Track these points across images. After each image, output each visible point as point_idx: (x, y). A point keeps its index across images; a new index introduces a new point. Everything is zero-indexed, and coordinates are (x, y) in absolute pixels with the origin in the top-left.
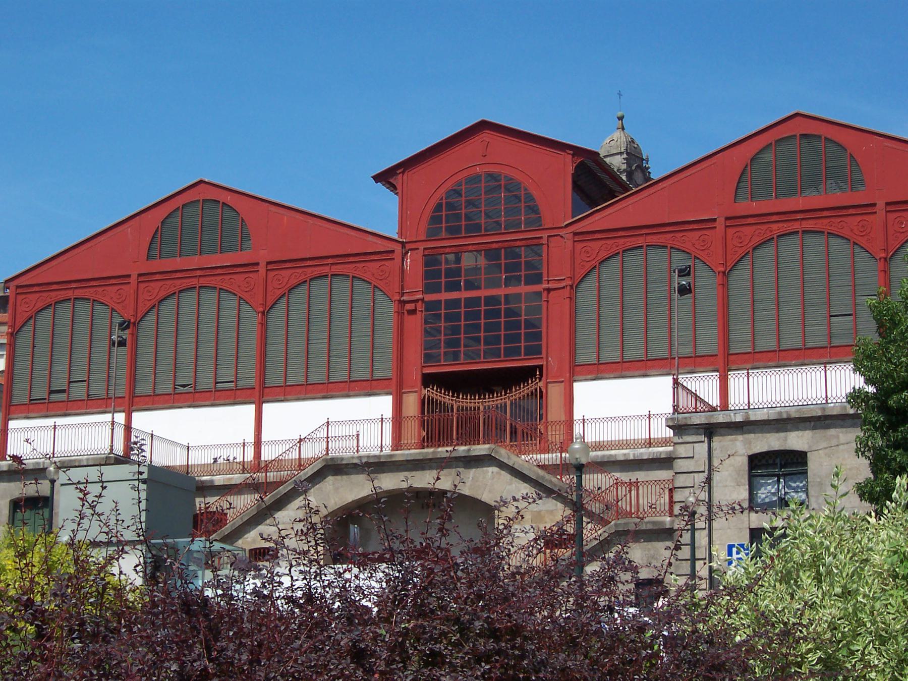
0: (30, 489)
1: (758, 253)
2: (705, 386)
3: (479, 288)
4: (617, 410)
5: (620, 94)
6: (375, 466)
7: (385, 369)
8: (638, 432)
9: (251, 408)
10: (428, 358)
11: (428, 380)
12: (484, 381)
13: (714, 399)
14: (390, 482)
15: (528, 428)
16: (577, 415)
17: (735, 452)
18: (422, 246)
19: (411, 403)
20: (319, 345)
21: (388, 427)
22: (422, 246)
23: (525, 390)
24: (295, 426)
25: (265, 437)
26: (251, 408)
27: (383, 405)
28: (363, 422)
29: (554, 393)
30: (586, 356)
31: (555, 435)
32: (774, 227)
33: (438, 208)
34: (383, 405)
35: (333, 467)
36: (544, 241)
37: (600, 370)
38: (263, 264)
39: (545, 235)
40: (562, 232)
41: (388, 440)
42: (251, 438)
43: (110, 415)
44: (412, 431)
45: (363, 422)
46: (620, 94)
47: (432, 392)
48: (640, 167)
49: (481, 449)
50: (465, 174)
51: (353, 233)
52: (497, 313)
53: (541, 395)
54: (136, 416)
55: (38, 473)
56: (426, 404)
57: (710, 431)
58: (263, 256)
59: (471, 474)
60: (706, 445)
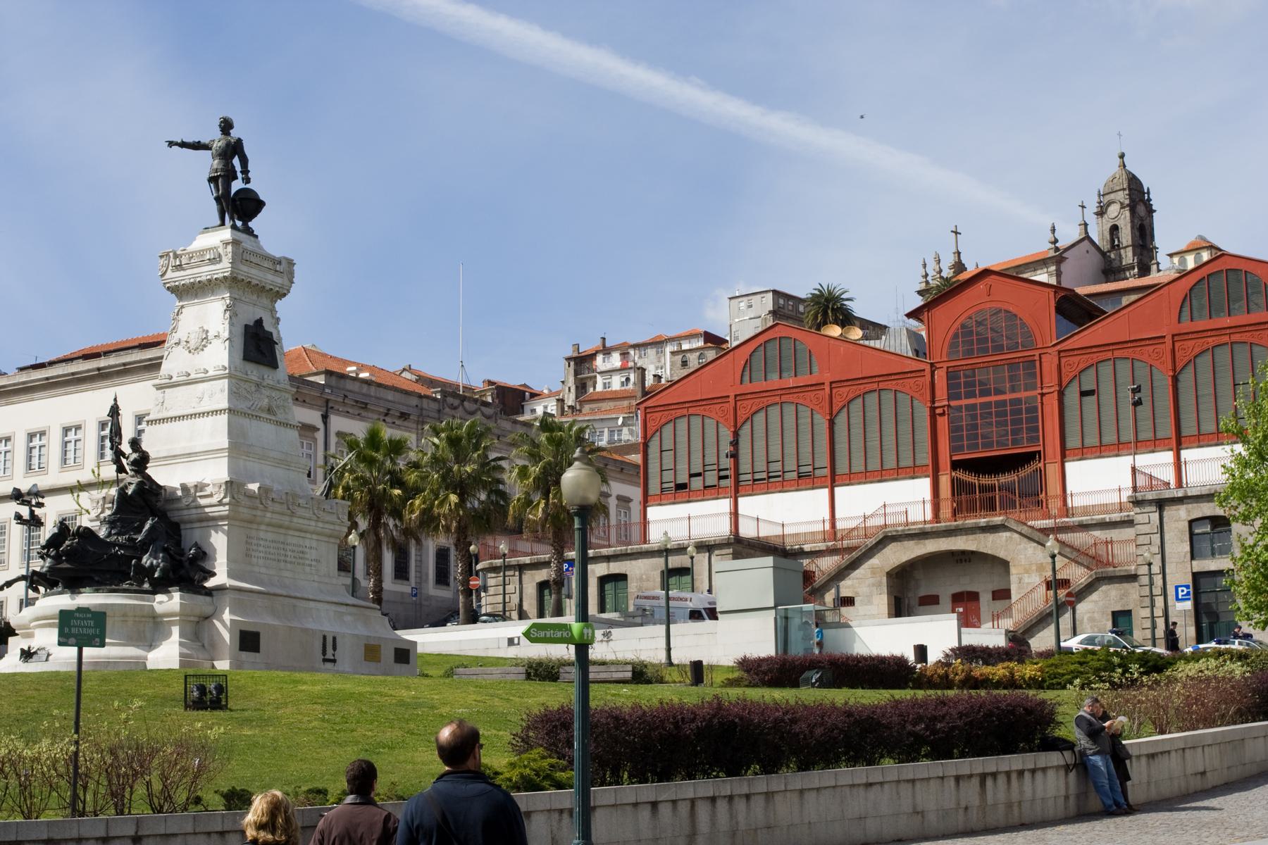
0: (675, 561)
1: (1199, 360)
2: (1158, 463)
3: (1003, 393)
4: (1095, 482)
5: (1120, 135)
6: (923, 535)
7: (925, 458)
8: (1114, 498)
9: (826, 491)
10: (953, 450)
11: (955, 465)
12: (996, 471)
13: (1168, 475)
14: (931, 546)
15: (1033, 495)
16: (1068, 492)
17: (1179, 517)
18: (945, 365)
19: (945, 481)
20: (874, 443)
21: (929, 507)
22: (945, 365)
23: (1025, 472)
24: (863, 504)
25: (837, 516)
26: (826, 491)
27: (921, 488)
28: (910, 499)
29: (1052, 470)
30: (1073, 442)
31: (1055, 505)
32: (1210, 340)
33: (956, 336)
34: (921, 488)
35: (888, 538)
36: (1037, 358)
37: (1084, 453)
38: (827, 384)
39: (1037, 353)
40: (1049, 351)
41: (929, 516)
42: (827, 517)
43: (724, 505)
44: (946, 511)
45: (910, 499)
46: (1120, 135)
47: (962, 475)
48: (1142, 200)
49: (998, 520)
50: (975, 309)
51: (893, 357)
52: (1004, 414)
53: (1041, 474)
54: (743, 502)
55: (681, 550)
56: (959, 488)
57: (1161, 504)
58: (827, 377)
59: (991, 537)
60: (1157, 515)
